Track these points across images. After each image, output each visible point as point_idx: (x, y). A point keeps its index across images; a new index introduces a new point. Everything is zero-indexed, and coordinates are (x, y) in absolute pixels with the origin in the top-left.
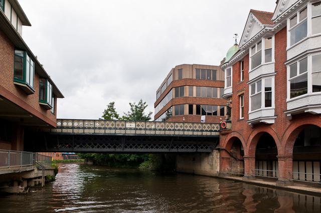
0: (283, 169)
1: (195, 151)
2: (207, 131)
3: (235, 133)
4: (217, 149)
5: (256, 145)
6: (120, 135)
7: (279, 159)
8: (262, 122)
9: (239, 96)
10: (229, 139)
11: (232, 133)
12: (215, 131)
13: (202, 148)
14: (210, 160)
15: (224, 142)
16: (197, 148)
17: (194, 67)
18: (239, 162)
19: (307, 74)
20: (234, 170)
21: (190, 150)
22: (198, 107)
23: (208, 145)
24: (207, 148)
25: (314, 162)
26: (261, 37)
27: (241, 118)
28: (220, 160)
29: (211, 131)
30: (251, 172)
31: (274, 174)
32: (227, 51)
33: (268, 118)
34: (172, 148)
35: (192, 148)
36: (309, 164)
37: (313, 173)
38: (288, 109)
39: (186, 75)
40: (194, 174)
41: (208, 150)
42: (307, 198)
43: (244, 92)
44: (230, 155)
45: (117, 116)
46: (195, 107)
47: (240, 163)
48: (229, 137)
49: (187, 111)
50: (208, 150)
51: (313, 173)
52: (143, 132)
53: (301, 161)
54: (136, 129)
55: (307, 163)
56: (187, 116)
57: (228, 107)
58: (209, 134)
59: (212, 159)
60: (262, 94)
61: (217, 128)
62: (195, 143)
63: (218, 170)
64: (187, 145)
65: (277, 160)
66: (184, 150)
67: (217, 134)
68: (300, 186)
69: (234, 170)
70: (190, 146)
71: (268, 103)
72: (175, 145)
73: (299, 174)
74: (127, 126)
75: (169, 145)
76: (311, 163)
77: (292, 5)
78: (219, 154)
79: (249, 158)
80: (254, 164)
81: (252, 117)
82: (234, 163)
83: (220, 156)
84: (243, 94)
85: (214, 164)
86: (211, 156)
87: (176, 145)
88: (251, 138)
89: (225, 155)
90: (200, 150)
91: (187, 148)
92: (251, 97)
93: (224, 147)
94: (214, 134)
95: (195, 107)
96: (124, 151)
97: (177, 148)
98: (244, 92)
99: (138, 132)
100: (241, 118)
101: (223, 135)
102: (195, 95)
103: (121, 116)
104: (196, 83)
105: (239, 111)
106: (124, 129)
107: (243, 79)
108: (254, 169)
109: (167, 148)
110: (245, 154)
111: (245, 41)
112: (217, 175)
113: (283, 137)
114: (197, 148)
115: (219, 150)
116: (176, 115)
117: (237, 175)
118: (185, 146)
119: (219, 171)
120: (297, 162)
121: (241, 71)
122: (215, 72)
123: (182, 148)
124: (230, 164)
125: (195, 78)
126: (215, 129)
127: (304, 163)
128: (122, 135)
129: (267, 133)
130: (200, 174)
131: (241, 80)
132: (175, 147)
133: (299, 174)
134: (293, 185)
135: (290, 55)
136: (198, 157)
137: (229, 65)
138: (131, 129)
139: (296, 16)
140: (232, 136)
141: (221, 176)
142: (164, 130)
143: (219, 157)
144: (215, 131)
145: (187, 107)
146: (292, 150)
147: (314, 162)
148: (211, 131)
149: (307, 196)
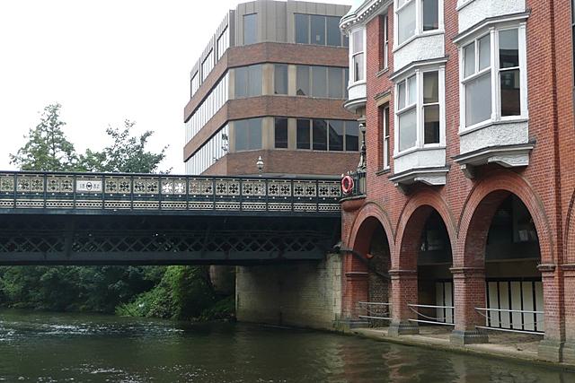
1: (275, 255)
2: (305, 200)
3: (374, 206)
6: (59, 212)
7: (543, 275)
8: (494, 163)
11: (367, 207)
13: (296, 248)
16: (282, 249)
19: (490, 70)
22: (302, 125)
24: (309, 248)
28: (342, 281)
31: (449, 314)
33: (431, 171)
34: (212, 248)
35: (268, 248)
36: (515, 285)
37: (510, 309)
38: (462, 152)
41: (314, 254)
45: (68, 148)
46: (292, 126)
48: (362, 218)
49: (268, 139)
50: (314, 254)
52: (124, 205)
53: (526, 279)
54: (103, 196)
56: (269, 151)
60: (418, 108)
65: (540, 279)
67: (334, 207)
70: (261, 242)
71: (510, 107)
74: (79, 188)
75: (202, 240)
80: (416, 289)
81: (400, 167)
84: (388, 102)
90: (288, 255)
91: (254, 248)
95: (292, 126)
96: (71, 259)
97: (226, 248)
99: (111, 205)
101: (349, 210)
102: (292, 92)
103: (80, 151)
106: (71, 196)
109: (197, 248)
110: (393, 265)
113: (460, 220)
114: (282, 249)
116: (436, 73)
119: (339, 312)
120: (519, 283)
128: (64, 213)
129: (512, 194)
130: (316, 326)
138: (89, 196)
145: (268, 127)
146: (483, 252)
147: (500, 283)
148: (318, 200)
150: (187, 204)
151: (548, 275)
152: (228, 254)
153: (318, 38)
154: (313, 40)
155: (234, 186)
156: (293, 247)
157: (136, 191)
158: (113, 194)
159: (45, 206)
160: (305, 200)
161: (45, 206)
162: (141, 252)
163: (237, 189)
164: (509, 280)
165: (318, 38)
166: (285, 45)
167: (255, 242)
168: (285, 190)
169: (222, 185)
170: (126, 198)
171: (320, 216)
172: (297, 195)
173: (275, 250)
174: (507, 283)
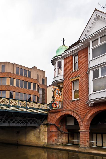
0: (84, 140)
1: (25, 125)
2: (38, 109)
4: (44, 124)
5: (91, 121)
7: (80, 133)
9: (72, 82)
10: (59, 116)
11: (64, 112)
12: (44, 110)
13: (31, 123)
14: (37, 133)
15: (53, 119)
16: (27, 123)
17: (15, 66)
18: (65, 134)
20: (60, 141)
21: (20, 125)
23: (36, 121)
24: (35, 123)
25: (97, 134)
26: (97, 35)
27: (73, 99)
28: (48, 133)
29: (41, 109)
30: (87, 144)
32: (57, 49)
34: (4, 122)
35: (23, 123)
37: (96, 141)
39: (8, 69)
40: (18, 145)
42: (98, 157)
43: (79, 78)
44: (58, 130)
47: (66, 136)
48: (60, 115)
51: (96, 141)
55: (97, 135)
57: (38, 97)
58: (39, 111)
59: (39, 133)
61: (46, 107)
62: (25, 119)
63: (46, 141)
64: (23, 121)
65: (79, 133)
66: (6, 125)
67: (46, 112)
68: (74, 148)
69: (60, 141)
70: (20, 121)
72: (7, 120)
73: (96, 143)
76: (100, 135)
77: (96, 31)
78: (47, 128)
79: (86, 132)
80: (89, 136)
82: (60, 135)
83: (48, 130)
85: (41, 136)
86: (38, 130)
87: (17, 120)
88: (89, 115)
89: (54, 129)
90: (29, 125)
91: (18, 123)
92: (92, 80)
93: (54, 123)
94: (43, 112)
97: (9, 122)
98: (79, 78)
100: (73, 99)
104: (17, 77)
105: (72, 93)
107: (75, 69)
108: (89, 141)
111: (86, 35)
112: (45, 146)
114: (27, 123)
115: (47, 125)
117: (63, 145)
118: (16, 121)
119: (47, 142)
120: (77, 134)
121: (73, 63)
122: (30, 72)
123: (14, 122)
124: (58, 136)
125: (15, 73)
126: (44, 108)
127: (95, 134)
131: (74, 70)
132: (7, 122)
133: (96, 143)
134: (90, 150)
135: (92, 65)
136: (26, 130)
137: (61, 58)
139: (98, 39)
140: (64, 114)
141: (50, 146)
142: (8, 106)
143: (47, 130)
144: (44, 110)
148: (41, 109)
149: (98, 156)
150: (18, 109)
151: (81, 133)
152: (9, 124)
153: (25, 75)
154: (24, 75)
155: (39, 105)
156: (13, 122)
157: (10, 104)
158: (44, 109)
159: (26, 111)
160: (38, 109)
161: (26, 111)
162: (19, 124)
163: (25, 104)
164: (96, 134)
165: (25, 75)
166: (13, 74)
167: (19, 121)
168: (16, 103)
169: (29, 104)
170: (25, 108)
171: (27, 113)
172: (28, 106)
173: (25, 124)
174: (77, 134)
